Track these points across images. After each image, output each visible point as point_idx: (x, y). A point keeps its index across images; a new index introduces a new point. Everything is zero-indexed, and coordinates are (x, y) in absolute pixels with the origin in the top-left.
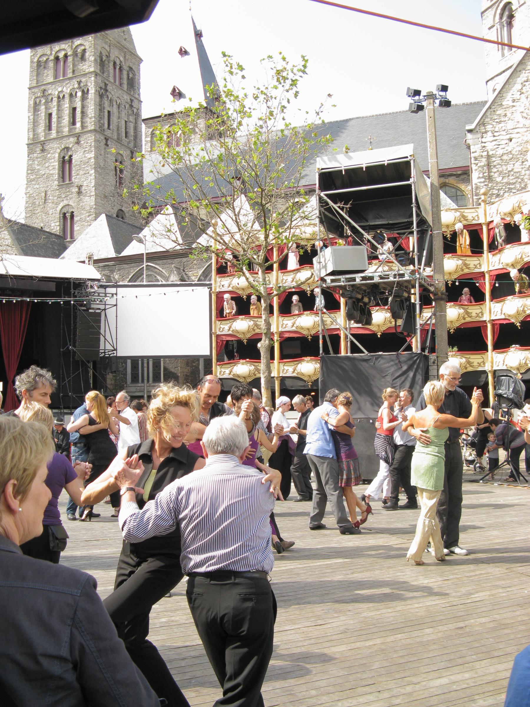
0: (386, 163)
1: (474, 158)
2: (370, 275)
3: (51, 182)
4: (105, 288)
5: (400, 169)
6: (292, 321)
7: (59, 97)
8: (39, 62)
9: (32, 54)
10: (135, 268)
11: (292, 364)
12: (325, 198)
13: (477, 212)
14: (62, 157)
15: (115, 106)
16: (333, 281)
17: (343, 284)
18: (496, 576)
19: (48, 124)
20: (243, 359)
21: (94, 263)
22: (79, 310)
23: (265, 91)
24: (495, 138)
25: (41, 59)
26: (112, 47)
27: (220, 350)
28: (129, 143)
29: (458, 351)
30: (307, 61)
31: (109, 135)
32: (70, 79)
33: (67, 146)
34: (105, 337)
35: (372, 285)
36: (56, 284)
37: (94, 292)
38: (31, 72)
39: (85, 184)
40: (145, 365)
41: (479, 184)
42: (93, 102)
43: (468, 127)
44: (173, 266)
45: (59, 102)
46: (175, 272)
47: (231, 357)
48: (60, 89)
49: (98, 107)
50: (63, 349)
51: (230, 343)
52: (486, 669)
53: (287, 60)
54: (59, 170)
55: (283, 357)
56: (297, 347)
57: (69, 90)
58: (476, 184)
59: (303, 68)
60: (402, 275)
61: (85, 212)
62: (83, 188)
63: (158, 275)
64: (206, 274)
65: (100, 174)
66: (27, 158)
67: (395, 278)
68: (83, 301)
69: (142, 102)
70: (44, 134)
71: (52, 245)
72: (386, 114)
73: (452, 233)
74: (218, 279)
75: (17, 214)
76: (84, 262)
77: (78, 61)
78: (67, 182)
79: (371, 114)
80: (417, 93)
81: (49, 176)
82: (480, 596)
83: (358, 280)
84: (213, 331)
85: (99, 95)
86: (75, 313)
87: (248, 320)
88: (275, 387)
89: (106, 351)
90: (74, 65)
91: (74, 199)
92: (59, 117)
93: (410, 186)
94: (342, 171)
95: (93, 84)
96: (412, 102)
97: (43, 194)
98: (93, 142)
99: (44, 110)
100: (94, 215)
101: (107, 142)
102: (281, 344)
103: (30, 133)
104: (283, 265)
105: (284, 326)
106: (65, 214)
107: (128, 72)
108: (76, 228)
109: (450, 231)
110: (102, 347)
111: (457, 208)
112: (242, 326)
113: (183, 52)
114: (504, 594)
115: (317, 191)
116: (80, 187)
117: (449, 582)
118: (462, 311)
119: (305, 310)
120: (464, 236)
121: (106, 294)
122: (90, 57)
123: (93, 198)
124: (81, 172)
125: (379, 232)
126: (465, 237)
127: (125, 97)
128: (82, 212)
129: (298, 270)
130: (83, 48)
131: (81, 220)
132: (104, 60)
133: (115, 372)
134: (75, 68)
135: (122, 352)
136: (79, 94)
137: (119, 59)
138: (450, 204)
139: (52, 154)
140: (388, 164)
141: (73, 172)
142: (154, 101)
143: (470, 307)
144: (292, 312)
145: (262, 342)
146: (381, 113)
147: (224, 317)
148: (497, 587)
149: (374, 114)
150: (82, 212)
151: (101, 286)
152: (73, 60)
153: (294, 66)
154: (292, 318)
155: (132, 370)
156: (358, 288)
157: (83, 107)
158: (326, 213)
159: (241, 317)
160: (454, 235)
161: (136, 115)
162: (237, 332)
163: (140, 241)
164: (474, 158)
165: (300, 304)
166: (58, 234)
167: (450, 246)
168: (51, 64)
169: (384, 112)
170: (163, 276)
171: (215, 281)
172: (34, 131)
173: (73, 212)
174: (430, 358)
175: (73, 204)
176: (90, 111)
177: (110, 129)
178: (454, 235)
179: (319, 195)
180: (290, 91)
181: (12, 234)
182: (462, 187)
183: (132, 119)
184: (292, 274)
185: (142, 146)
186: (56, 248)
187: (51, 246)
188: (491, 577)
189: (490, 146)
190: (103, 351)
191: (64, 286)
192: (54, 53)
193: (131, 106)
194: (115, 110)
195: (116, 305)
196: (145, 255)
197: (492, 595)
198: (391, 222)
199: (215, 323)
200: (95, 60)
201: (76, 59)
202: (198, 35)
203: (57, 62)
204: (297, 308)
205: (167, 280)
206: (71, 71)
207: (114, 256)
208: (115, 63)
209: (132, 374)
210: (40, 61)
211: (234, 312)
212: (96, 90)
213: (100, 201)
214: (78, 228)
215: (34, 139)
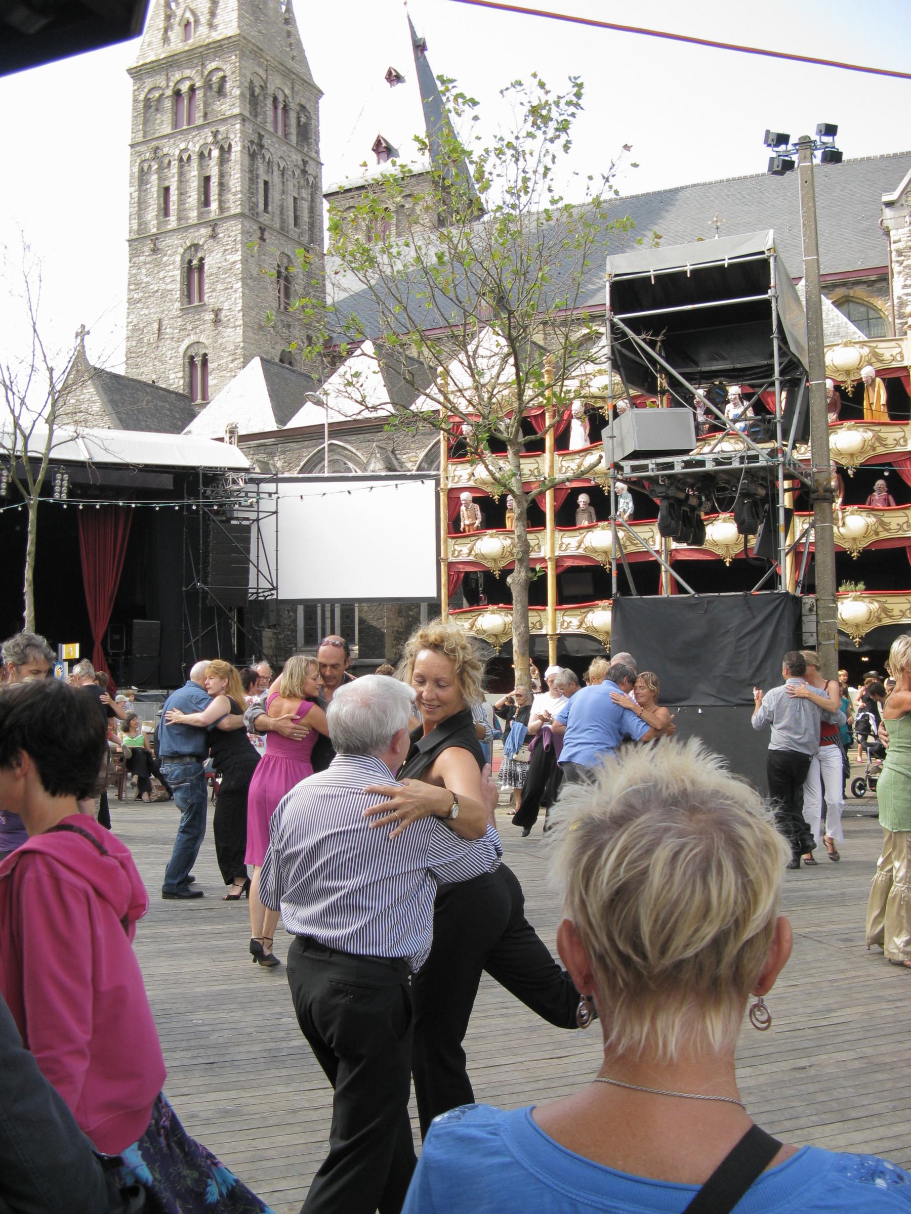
0: (726, 263)
1: (897, 251)
2: (699, 458)
3: (168, 305)
4: (258, 484)
5: (753, 273)
6: (578, 538)
7: (181, 160)
8: (147, 100)
9: (136, 88)
10: (310, 450)
11: (578, 612)
12: (622, 325)
13: (900, 347)
14: (186, 261)
15: (276, 173)
16: (634, 469)
17: (650, 473)
18: (882, 981)
19: (162, 205)
20: (493, 604)
21: (239, 442)
22: (214, 521)
23: (514, 142)
25: (151, 96)
26: (270, 72)
27: (454, 588)
28: (301, 234)
29: (866, 590)
30: (580, 86)
31: (267, 222)
32: (199, 128)
33: (196, 242)
34: (257, 567)
35: (703, 476)
36: (175, 479)
37: (239, 491)
38: (135, 117)
39: (226, 306)
40: (328, 614)
41: (905, 298)
42: (238, 167)
43: (886, 198)
44: (374, 444)
45: (181, 167)
46: (378, 455)
47: (474, 600)
48: (182, 146)
49: (247, 175)
50: (187, 586)
51: (472, 576)
52: (831, 1140)
53: (547, 87)
54: (182, 284)
55: (562, 600)
56: (583, 582)
57: (198, 146)
58: (899, 298)
59: (575, 100)
60: (755, 458)
61: (226, 354)
62: (224, 313)
63: (350, 460)
64: (431, 458)
65: (251, 289)
66: (128, 264)
67: (742, 463)
68: (212, 506)
69: (322, 164)
70: (156, 222)
71: (171, 410)
72: (745, 178)
73: (855, 383)
74: (450, 466)
75: (103, 359)
76: (221, 440)
77: (213, 97)
78: (196, 304)
79: (718, 178)
80: (783, 139)
81: (165, 293)
82: (846, 1014)
83: (678, 469)
84: (442, 556)
85: (250, 155)
86: (206, 526)
87: (501, 537)
88: (548, 652)
89: (260, 591)
90: (206, 105)
91: (207, 332)
92: (182, 194)
93: (767, 303)
94: (649, 278)
95: (239, 135)
96: (774, 155)
97: (156, 326)
98: (240, 235)
99: (156, 182)
100: (242, 360)
101: (262, 234)
102: (559, 578)
103: (134, 221)
104: (562, 442)
105: (564, 546)
106: (192, 358)
107: (298, 113)
108: (212, 381)
109: (853, 381)
110: (252, 583)
111: (866, 339)
112: (491, 546)
113: (394, 78)
114: (889, 1013)
115: (608, 314)
116: (217, 312)
117: (796, 989)
118: (872, 520)
119: (599, 520)
120: (876, 389)
121: (258, 493)
122: (233, 89)
123: (240, 331)
124: (220, 287)
125: (717, 383)
126: (879, 392)
127: (294, 157)
128: (222, 354)
129: (585, 451)
130: (221, 74)
131: (219, 368)
132: (256, 94)
133: (274, 626)
134: (209, 109)
135: (286, 593)
136: (215, 153)
137: (283, 91)
138: (854, 333)
139: (170, 256)
140: (730, 265)
141: (206, 286)
142: (343, 160)
143: (887, 514)
144: (578, 522)
145: (514, 574)
146: (736, 176)
147: (461, 532)
148: (880, 999)
149: (724, 178)
150: (222, 354)
151: (251, 481)
152: (205, 95)
153: (559, 97)
154: (577, 533)
155: (306, 624)
156: (679, 481)
157: (222, 175)
158: (624, 351)
159: (489, 532)
160: (860, 387)
161: (312, 187)
162: (484, 557)
163: (319, 403)
164: (897, 251)
165: (592, 509)
166: (181, 392)
167: (849, 404)
168: (168, 104)
169: (742, 174)
170: (357, 463)
171: (446, 470)
172: (140, 218)
173: (205, 355)
174: (804, 601)
175: (206, 342)
176: (233, 182)
177: (267, 213)
178: (860, 387)
179: (611, 320)
180: (557, 141)
181: (103, 394)
182: (879, 303)
183: (305, 193)
184: (577, 457)
185: (323, 239)
186: (177, 416)
187: (168, 413)
188: (872, 982)
190: (255, 591)
191: (188, 479)
192: (172, 84)
193: (304, 172)
194: (276, 179)
195: (276, 512)
196: (326, 426)
197: (868, 1013)
198: (738, 366)
199: (446, 542)
200: (242, 95)
201: (209, 94)
202: (420, 47)
203: (177, 100)
204: (586, 515)
205: (365, 470)
206: (202, 114)
207: (275, 429)
208: (275, 99)
209: (306, 630)
210: (149, 99)
211: (478, 522)
212: (244, 147)
213: (251, 334)
214: (215, 382)
215: (139, 231)
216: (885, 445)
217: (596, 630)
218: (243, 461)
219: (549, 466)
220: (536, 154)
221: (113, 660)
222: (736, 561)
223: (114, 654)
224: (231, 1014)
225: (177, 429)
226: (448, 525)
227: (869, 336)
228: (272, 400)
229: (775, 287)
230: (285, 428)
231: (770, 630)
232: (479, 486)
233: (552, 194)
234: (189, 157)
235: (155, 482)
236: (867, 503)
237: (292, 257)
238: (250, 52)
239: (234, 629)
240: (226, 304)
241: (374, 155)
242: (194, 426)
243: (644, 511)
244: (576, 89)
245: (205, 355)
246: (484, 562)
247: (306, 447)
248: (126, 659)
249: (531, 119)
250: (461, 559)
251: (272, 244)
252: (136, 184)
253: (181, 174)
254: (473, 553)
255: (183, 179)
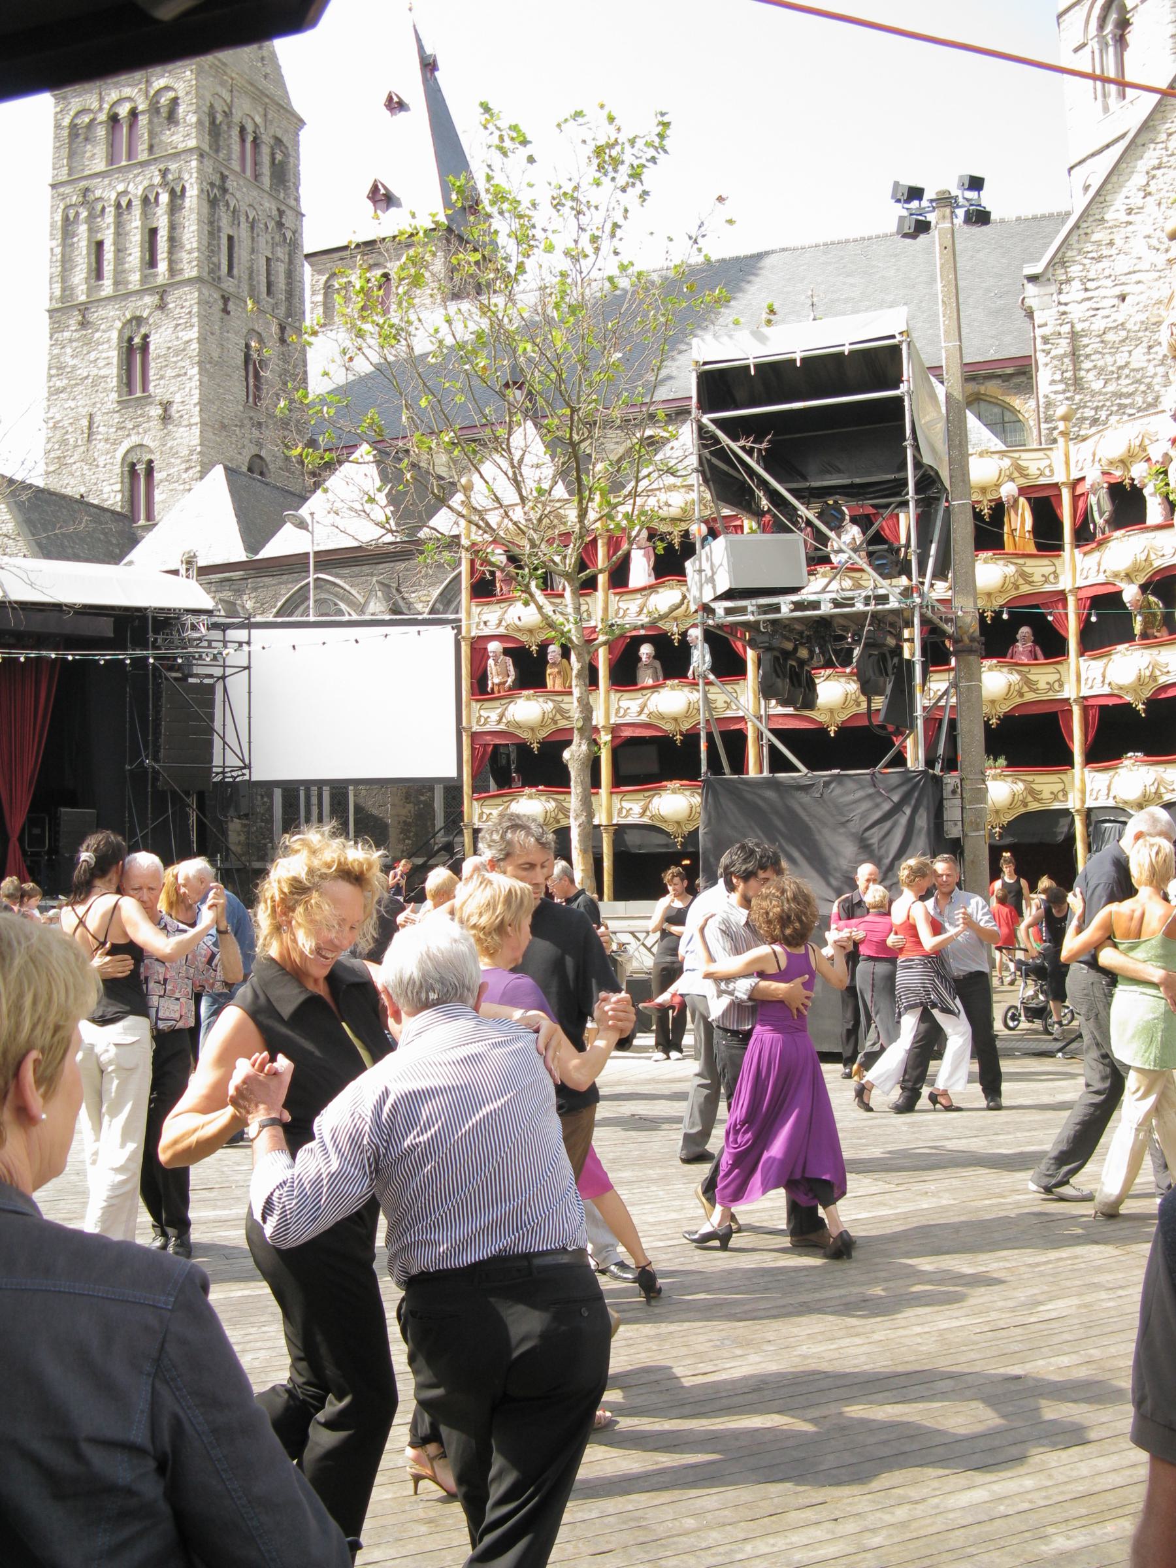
1: (1043, 337)
3: (101, 395)
4: (224, 631)
5: (879, 363)
7: (118, 206)
8: (73, 126)
9: (58, 109)
10: (290, 586)
11: (640, 796)
12: (712, 427)
13: (1049, 458)
14: (126, 338)
16: (729, 611)
17: (751, 618)
19: (94, 265)
21: (198, 575)
22: (167, 679)
24: (1089, 294)
25: (78, 121)
26: (235, 93)
27: (479, 766)
29: (1007, 766)
30: (666, 125)
31: (231, 290)
32: (143, 164)
33: (138, 314)
36: (115, 622)
37: (200, 639)
39: (178, 398)
40: (314, 800)
41: (1052, 396)
42: (194, 216)
43: (1030, 270)
44: (375, 579)
45: (119, 215)
46: (379, 594)
47: (504, 781)
48: (121, 187)
49: (206, 227)
50: (131, 765)
52: (1072, 1469)
54: (120, 368)
55: (620, 780)
57: (141, 188)
58: (1046, 396)
59: (657, 140)
60: (884, 599)
61: (178, 461)
62: (175, 407)
63: (342, 599)
64: (448, 598)
65: (211, 377)
66: (48, 342)
67: (867, 605)
70: (85, 287)
73: (993, 504)
74: (474, 608)
76: (175, 572)
77: (161, 124)
78: (139, 395)
80: (915, 193)
83: (785, 610)
84: (464, 724)
86: (157, 686)
87: (541, 699)
88: (601, 847)
89: (227, 770)
90: (152, 134)
91: (153, 432)
92: (120, 250)
93: (899, 400)
94: (748, 367)
95: (195, 175)
96: (905, 213)
97: (85, 422)
98: (196, 306)
99: (85, 235)
100: (198, 468)
104: (619, 577)
106: (133, 465)
107: (272, 148)
108: (159, 496)
109: (990, 501)
110: (217, 760)
111: (1005, 448)
112: (527, 712)
113: (395, 105)
114: (1111, 1304)
115: (694, 411)
116: (166, 406)
118: (1015, 678)
120: (1020, 511)
122: (188, 114)
123: (196, 431)
124: (170, 373)
125: (831, 502)
127: (267, 205)
128: (173, 460)
130: (171, 95)
131: (169, 479)
132: (218, 122)
133: (246, 815)
135: (260, 773)
136: (164, 198)
137: (253, 119)
139: (104, 331)
140: (851, 352)
141: (152, 372)
143: (1034, 670)
144: (639, 680)
145: (573, 747)
147: (488, 694)
148: (1097, 1287)
151: (215, 626)
152: (150, 122)
154: (638, 695)
155: (285, 812)
156: (785, 627)
157: (173, 227)
158: (715, 461)
159: (525, 692)
160: (999, 509)
161: (290, 245)
163: (302, 525)
164: (1043, 337)
165: (657, 664)
167: (989, 533)
168: (101, 132)
170: (351, 603)
171: (469, 613)
173: (151, 461)
174: (945, 781)
178: (999, 509)
179: (699, 421)
181: (15, 510)
182: (1017, 402)
183: (281, 253)
185: (304, 313)
187: (102, 537)
188: (1083, 1266)
189: (1077, 312)
190: (220, 770)
191: (133, 624)
192: (106, 106)
193: (280, 225)
194: (243, 233)
195: (248, 668)
196: (312, 555)
197: (1085, 1306)
198: (857, 481)
199: (469, 705)
201: (155, 120)
202: (429, 66)
203: (113, 128)
204: (650, 671)
205: (362, 612)
206: (146, 146)
207: (245, 559)
208: (243, 129)
211: (510, 681)
214: (163, 496)
215: (63, 299)
216: (1030, 583)
217: (664, 820)
218: (205, 601)
219: (604, 609)
220: (603, 208)
221: (32, 861)
222: (843, 730)
223: (34, 854)
224: (264, 1329)
225: (114, 558)
226: (472, 684)
227: (1005, 443)
228: (239, 522)
229: (908, 381)
230: (260, 556)
231: (903, 820)
232: (511, 633)
233: (618, 258)
234: (130, 202)
235: (91, 628)
236: (1009, 655)
237: (264, 335)
238: (211, 67)
239: (193, 819)
240: (178, 395)
241: (370, 204)
242: (135, 555)
243: (728, 665)
244: (661, 128)
245: (151, 461)
246: (518, 732)
247: (285, 583)
248: (50, 860)
249: (595, 162)
250: (487, 728)
251: (238, 318)
252: (59, 236)
253: (119, 224)
254: (504, 720)
255: (121, 232)
